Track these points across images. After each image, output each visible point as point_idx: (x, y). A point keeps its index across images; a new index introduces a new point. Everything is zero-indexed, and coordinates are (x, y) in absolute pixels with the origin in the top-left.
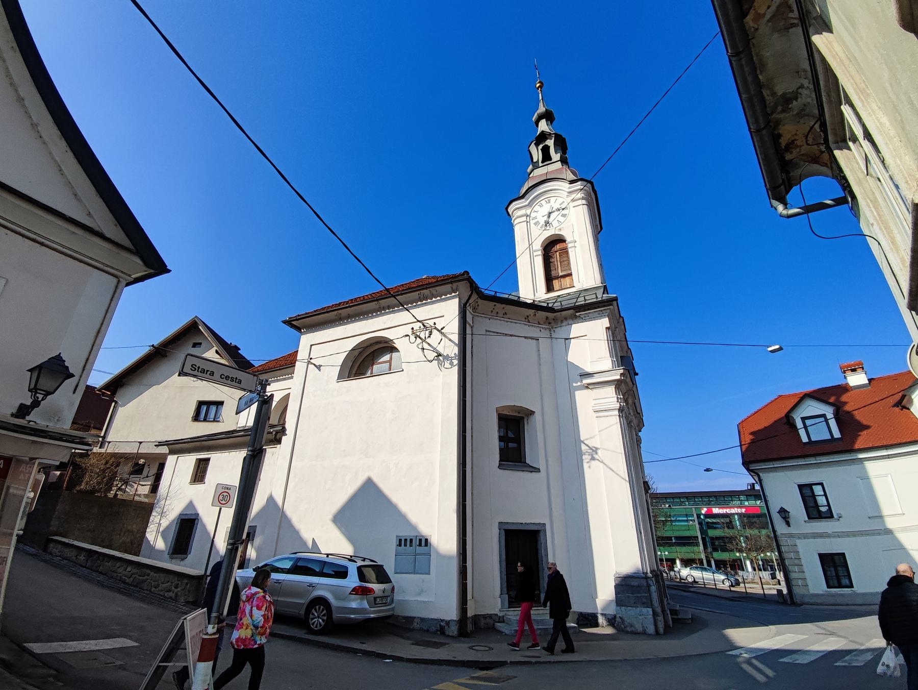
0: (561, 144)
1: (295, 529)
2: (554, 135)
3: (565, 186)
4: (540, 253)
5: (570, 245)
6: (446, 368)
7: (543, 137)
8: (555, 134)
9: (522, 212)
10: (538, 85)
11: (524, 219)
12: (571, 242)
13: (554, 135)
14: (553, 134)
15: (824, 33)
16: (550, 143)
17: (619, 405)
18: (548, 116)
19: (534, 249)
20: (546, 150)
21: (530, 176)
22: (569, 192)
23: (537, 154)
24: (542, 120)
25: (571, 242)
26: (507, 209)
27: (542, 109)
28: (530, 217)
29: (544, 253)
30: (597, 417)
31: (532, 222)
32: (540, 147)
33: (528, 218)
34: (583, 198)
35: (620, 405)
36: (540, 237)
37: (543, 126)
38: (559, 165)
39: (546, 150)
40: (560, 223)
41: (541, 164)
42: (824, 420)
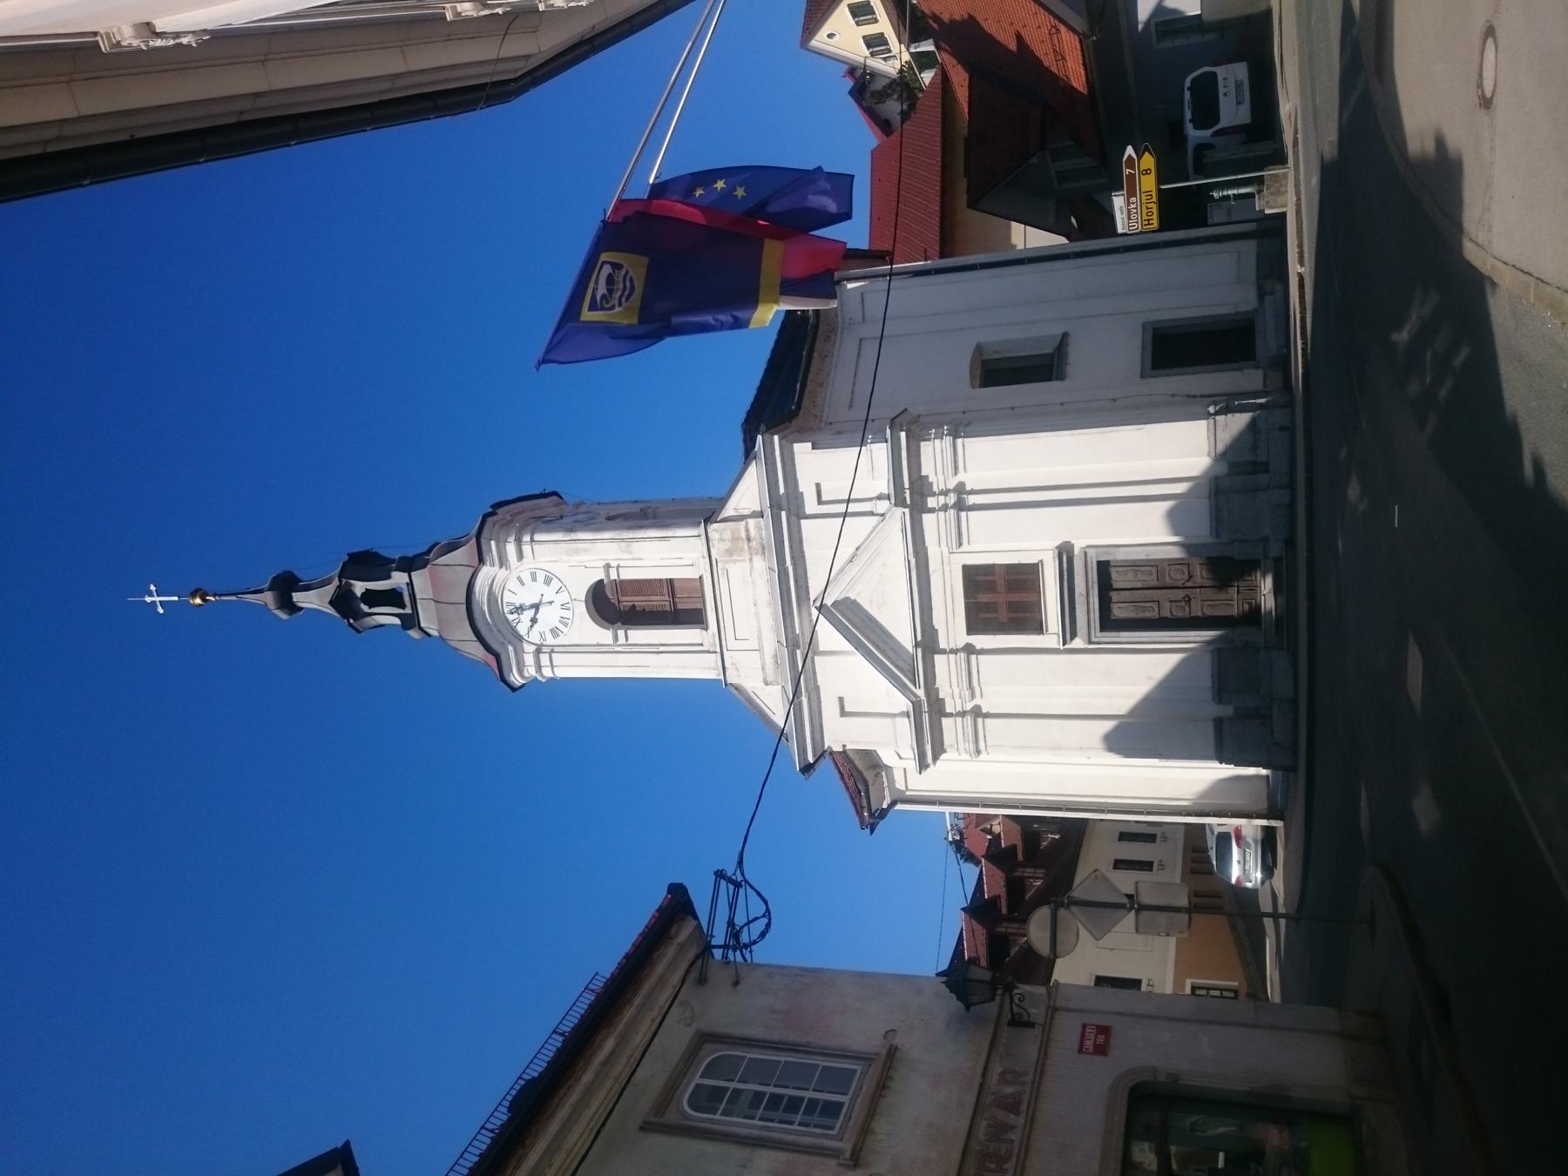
0: (366, 563)
1: (1036, 908)
2: (344, 581)
3: (486, 573)
4: (621, 633)
5: (614, 576)
6: (765, 902)
7: (344, 602)
8: (340, 577)
9: (529, 659)
10: (198, 601)
11: (544, 659)
12: (608, 575)
13: (344, 581)
14: (340, 581)
15: (801, 490)
16: (359, 587)
17: (948, 437)
18: (286, 586)
19: (611, 642)
20: (373, 598)
21: (434, 633)
22: (501, 566)
23: (386, 617)
24: (295, 600)
25: (608, 575)
26: (513, 689)
27: (268, 598)
28: (542, 645)
29: (619, 624)
30: (965, 471)
31: (550, 640)
32: (365, 608)
33: (544, 649)
34: (519, 541)
35: (946, 435)
36: (591, 631)
37: (312, 601)
38: (420, 578)
39: (373, 598)
40: (563, 588)
41: (408, 610)
42: (975, 656)
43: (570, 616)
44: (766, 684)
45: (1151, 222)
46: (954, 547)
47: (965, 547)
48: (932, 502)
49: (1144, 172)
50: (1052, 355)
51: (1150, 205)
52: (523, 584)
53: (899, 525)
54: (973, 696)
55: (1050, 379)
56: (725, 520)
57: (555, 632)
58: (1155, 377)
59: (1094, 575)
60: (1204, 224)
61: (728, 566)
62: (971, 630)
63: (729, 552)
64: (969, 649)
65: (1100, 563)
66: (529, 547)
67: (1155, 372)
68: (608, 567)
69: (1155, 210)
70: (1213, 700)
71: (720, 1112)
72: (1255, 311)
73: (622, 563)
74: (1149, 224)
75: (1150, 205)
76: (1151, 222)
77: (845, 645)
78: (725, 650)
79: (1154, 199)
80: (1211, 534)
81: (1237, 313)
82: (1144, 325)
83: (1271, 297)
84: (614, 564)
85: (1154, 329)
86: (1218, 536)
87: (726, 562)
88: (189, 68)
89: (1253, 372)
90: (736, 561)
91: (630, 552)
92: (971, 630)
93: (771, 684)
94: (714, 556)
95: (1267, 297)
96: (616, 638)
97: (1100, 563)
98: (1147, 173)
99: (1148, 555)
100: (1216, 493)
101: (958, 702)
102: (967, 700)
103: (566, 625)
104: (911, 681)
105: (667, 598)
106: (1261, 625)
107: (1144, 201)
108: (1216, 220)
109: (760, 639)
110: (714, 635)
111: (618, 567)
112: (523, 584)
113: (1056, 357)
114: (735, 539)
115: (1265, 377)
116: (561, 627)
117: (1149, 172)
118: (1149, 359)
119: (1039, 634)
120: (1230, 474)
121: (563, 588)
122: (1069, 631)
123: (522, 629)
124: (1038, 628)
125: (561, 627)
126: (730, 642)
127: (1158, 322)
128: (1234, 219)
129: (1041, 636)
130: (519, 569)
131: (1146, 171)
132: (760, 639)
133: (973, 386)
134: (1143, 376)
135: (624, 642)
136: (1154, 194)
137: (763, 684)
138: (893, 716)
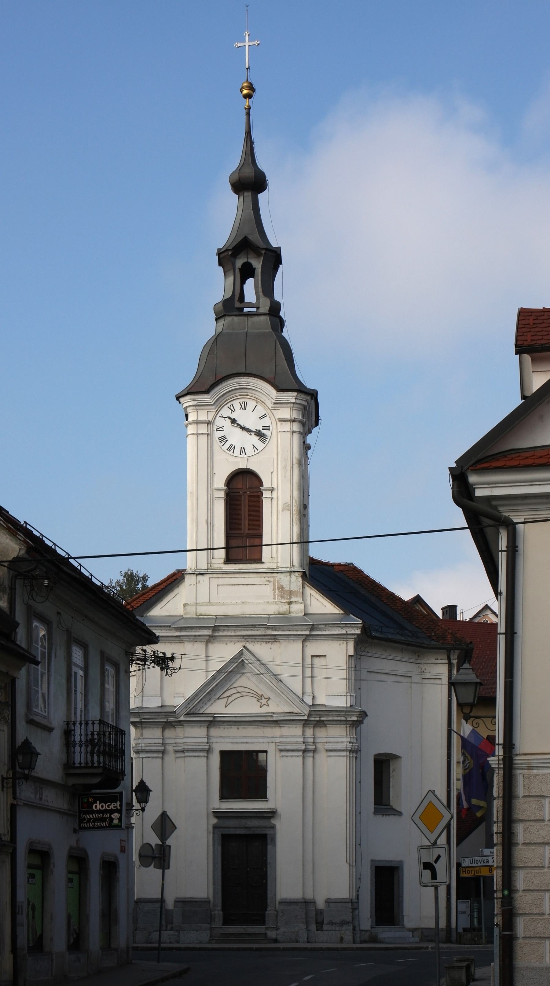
9: (203, 416)
25: (266, 489)
40: (257, 452)
43: (235, 454)
44: (185, 606)
45: (464, 873)
46: (280, 747)
47: (278, 754)
48: (309, 732)
49: (490, 869)
50: (389, 805)
51: (473, 872)
52: (261, 418)
53: (296, 710)
54: (176, 752)
55: (375, 804)
56: (303, 587)
57: (223, 439)
58: (371, 868)
59: (259, 831)
60: (458, 898)
61: (272, 584)
62: (223, 754)
63: (281, 588)
64: (208, 751)
65: (266, 835)
66: (289, 430)
67: (374, 868)
68: (272, 490)
69: (470, 875)
70: (177, 898)
71: (42, 670)
72: (403, 927)
73: (275, 501)
74: (463, 871)
75: (473, 872)
76: (464, 873)
77: (216, 666)
78: (210, 576)
79: (476, 874)
80: (281, 899)
81: (403, 916)
82: (401, 862)
83: (411, 935)
84: (274, 494)
85: (398, 867)
86: (280, 903)
87: (274, 585)
88: (520, 747)
89: (369, 924)
90: (274, 593)
91: (283, 510)
92: (223, 754)
93: (185, 609)
94: (279, 575)
95: (411, 933)
96: (218, 490)
97: (266, 835)
98: (490, 870)
99: (270, 863)
100: (305, 902)
101: (173, 741)
102: (175, 748)
103: (229, 449)
104: (188, 712)
105: (246, 531)
106: (223, 925)
107: (475, 869)
108: (459, 904)
109: (218, 604)
110: (220, 569)
111: (272, 498)
112: (261, 418)
113: (388, 807)
114: (290, 593)
115: (366, 931)
116: (227, 445)
117: (491, 871)
118: (381, 864)
119: (220, 797)
120: (317, 910)
121: (257, 452)
122: (218, 815)
123: (225, 412)
124: (223, 796)
125: (227, 445)
126: (215, 581)
127: (403, 869)
128: (459, 915)
129: (219, 798)
130: (273, 418)
131: (491, 870)
132: (218, 604)
133: (375, 756)
134: (373, 861)
135: (216, 496)
136: (479, 874)
137: (185, 602)
138: (161, 696)
